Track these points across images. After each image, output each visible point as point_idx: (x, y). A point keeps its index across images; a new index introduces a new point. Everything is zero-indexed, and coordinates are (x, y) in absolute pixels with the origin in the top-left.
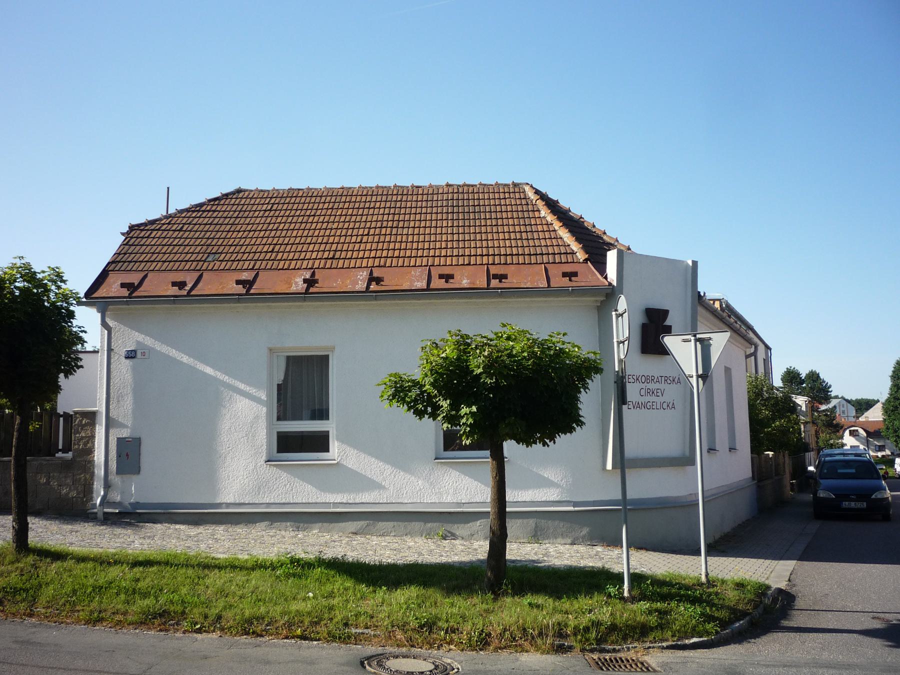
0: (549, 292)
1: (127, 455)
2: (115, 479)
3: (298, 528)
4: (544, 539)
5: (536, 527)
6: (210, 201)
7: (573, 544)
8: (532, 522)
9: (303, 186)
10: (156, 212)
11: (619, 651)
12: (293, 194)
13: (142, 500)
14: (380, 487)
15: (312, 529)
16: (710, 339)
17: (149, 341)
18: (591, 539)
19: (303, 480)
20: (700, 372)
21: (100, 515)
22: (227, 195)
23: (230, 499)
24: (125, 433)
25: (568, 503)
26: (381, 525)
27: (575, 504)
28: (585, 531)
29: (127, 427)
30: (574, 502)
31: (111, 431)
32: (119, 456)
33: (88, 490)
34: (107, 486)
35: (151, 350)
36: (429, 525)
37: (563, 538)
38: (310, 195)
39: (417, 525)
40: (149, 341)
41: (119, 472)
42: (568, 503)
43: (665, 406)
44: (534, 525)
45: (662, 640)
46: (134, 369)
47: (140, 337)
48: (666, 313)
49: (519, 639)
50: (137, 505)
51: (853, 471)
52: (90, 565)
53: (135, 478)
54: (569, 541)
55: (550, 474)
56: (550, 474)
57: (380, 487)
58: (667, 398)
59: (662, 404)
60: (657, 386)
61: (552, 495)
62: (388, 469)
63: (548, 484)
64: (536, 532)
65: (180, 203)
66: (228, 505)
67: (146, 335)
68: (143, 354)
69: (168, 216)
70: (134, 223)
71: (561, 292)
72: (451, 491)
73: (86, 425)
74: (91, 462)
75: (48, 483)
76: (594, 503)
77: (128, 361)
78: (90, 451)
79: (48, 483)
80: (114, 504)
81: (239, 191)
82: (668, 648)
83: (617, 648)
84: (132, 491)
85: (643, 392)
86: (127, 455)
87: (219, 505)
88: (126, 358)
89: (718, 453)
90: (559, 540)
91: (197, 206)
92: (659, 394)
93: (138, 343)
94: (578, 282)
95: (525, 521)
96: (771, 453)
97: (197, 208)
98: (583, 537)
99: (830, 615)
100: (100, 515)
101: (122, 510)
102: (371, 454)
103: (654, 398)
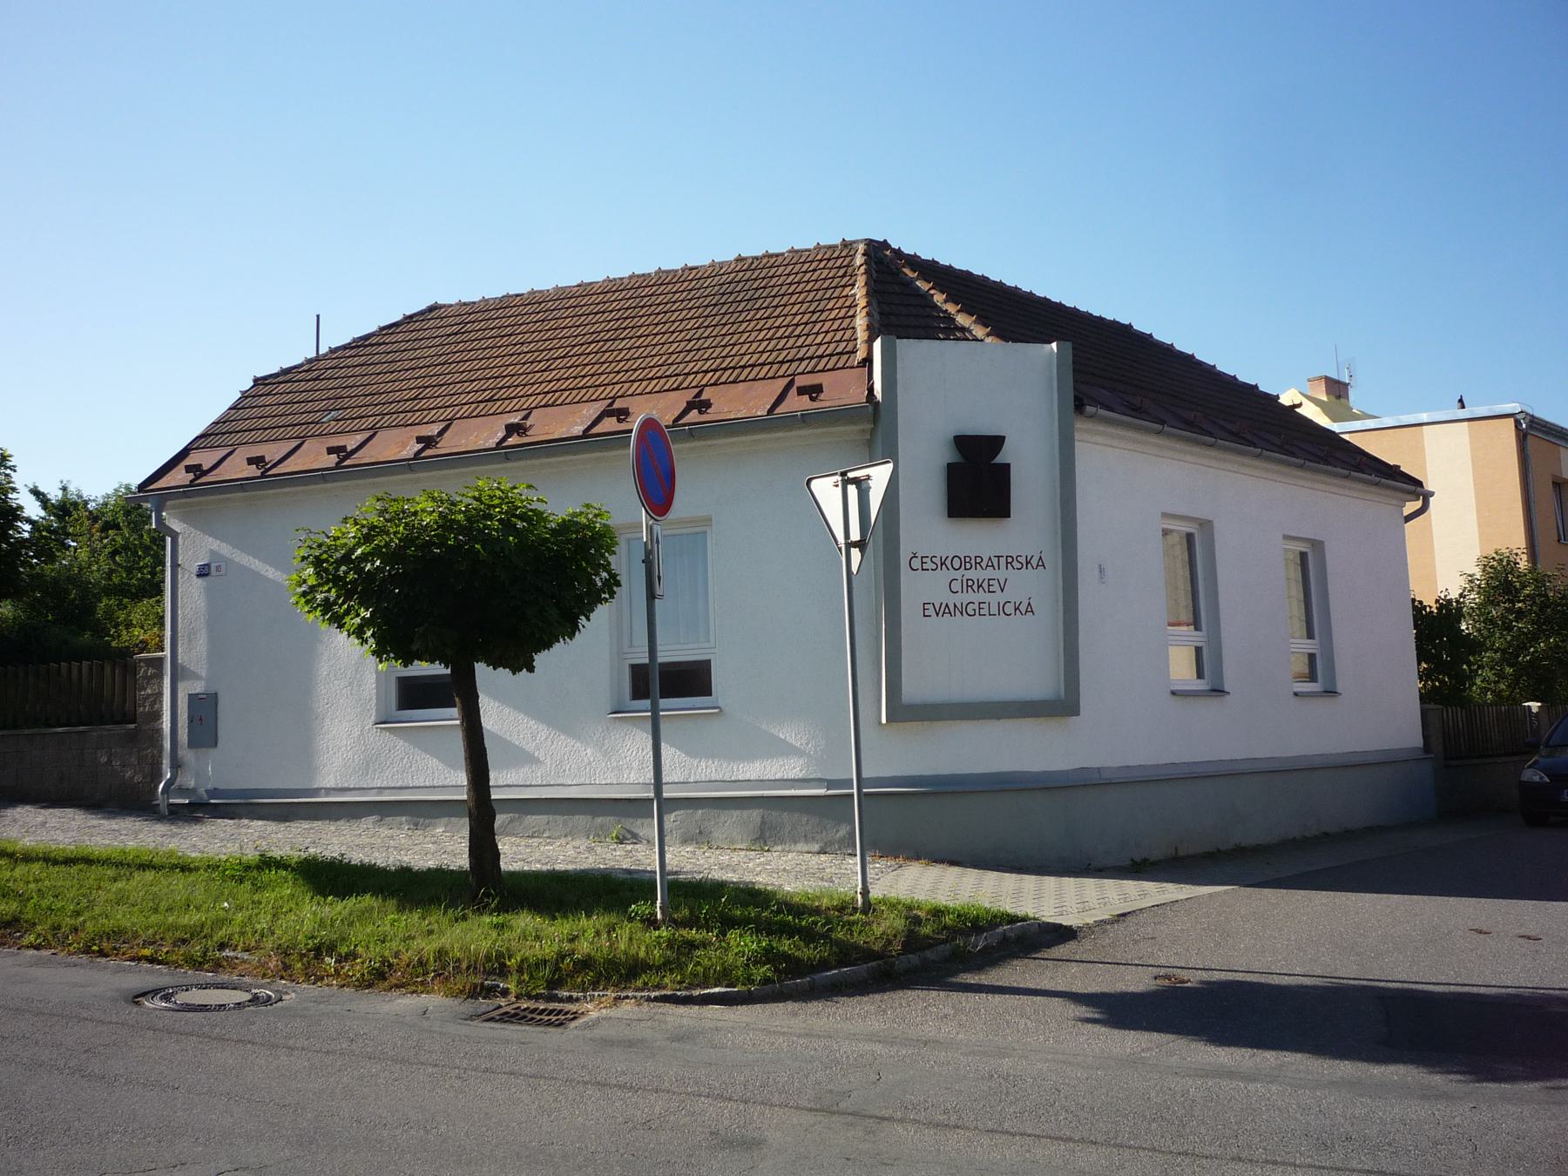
0: (772, 422)
1: (1101, 570)
2: (186, 754)
3: (416, 824)
4: (775, 844)
5: (763, 823)
6: (382, 329)
7: (822, 852)
8: (755, 815)
9: (524, 290)
10: (297, 352)
11: (577, 1000)
12: (507, 303)
13: (222, 786)
14: (532, 760)
15: (435, 826)
16: (869, 477)
17: (225, 549)
19: (426, 751)
20: (855, 535)
21: (164, 809)
22: (411, 317)
23: (329, 782)
24: (198, 687)
25: (819, 782)
26: (531, 820)
29: (197, 677)
30: (828, 781)
31: (181, 686)
32: (191, 720)
33: (156, 775)
34: (176, 765)
35: (228, 561)
36: (599, 820)
37: (807, 841)
38: (535, 301)
39: (581, 820)
40: (225, 549)
41: (192, 744)
42: (819, 782)
43: (1009, 609)
44: (759, 820)
45: (658, 987)
46: (209, 593)
47: (214, 544)
48: (997, 442)
49: (418, 975)
50: (214, 793)
52: (36, 868)
53: (212, 753)
54: (816, 847)
55: (790, 734)
56: (790, 734)
57: (532, 760)
58: (1014, 594)
59: (1002, 609)
60: (990, 573)
61: (792, 768)
62: (543, 731)
63: (787, 750)
64: (762, 831)
65: (336, 337)
66: (329, 791)
67: (222, 540)
68: (218, 568)
69: (317, 359)
70: (259, 375)
71: (805, 419)
72: (635, 765)
73: (151, 677)
74: (159, 731)
75: (109, 762)
77: (200, 581)
78: (157, 716)
79: (109, 762)
80: (183, 791)
81: (432, 309)
82: (656, 999)
83: (575, 995)
84: (209, 771)
85: (956, 586)
86: (1101, 570)
87: (316, 792)
88: (199, 576)
89: (1227, 697)
90: (801, 846)
91: (361, 338)
92: (996, 587)
93: (212, 552)
94: (828, 400)
95: (746, 813)
96: (1535, 706)
97: (362, 343)
99: (1074, 968)
100: (164, 809)
101: (194, 799)
102: (517, 708)
103: (982, 596)
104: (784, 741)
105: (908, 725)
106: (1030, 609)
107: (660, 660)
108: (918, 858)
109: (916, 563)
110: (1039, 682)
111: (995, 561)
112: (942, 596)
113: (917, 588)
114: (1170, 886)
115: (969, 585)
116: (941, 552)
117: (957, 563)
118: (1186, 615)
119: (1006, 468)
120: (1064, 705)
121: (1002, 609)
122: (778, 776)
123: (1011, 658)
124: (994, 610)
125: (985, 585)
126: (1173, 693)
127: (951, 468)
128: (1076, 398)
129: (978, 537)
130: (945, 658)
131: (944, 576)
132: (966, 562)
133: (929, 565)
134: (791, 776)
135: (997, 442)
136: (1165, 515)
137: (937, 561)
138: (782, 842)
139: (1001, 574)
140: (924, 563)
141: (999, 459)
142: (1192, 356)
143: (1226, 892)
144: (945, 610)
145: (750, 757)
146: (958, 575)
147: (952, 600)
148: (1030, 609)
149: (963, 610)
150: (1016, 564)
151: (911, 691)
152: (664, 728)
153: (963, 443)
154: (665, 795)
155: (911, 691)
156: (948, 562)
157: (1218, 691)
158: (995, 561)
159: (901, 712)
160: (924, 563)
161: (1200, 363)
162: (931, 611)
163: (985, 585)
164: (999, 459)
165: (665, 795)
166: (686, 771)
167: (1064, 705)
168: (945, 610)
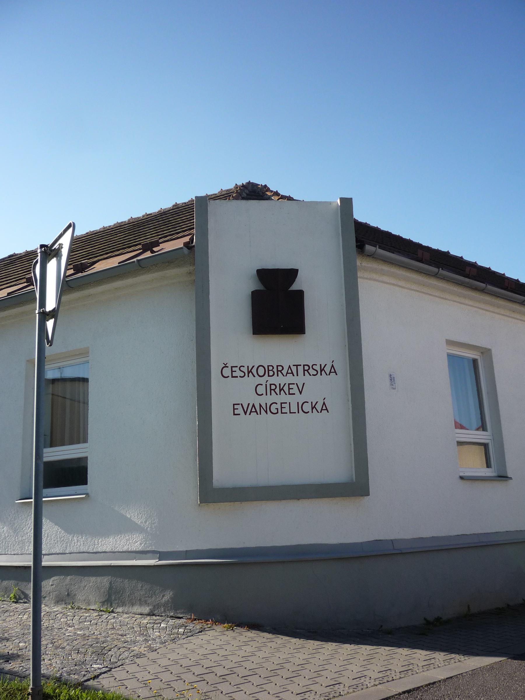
1: (392, 379)
4: (118, 606)
5: (111, 588)
7: (151, 614)
8: (105, 581)
18: (176, 608)
25: (142, 554)
27: (162, 555)
28: (168, 595)
30: (159, 552)
37: (141, 605)
43: (307, 407)
44: (107, 585)
48: (292, 274)
51: (44, 499)
54: (146, 610)
56: (134, 514)
59: (300, 407)
60: (290, 379)
61: (135, 542)
63: (129, 527)
64: (110, 596)
76: (187, 554)
85: (261, 390)
86: (392, 379)
90: (137, 609)
92: (295, 390)
95: (99, 579)
98: (165, 605)
104: (130, 519)
105: (222, 505)
106: (325, 408)
107: (45, 459)
108: (222, 622)
109: (227, 372)
110: (335, 467)
111: (294, 369)
112: (249, 398)
113: (225, 393)
114: (440, 656)
115: (272, 389)
116: (249, 362)
117: (261, 371)
118: (475, 421)
119: (301, 293)
120: (355, 487)
121: (300, 407)
122: (125, 549)
123: (311, 447)
124: (294, 409)
125: (286, 388)
126: (462, 478)
127: (255, 295)
128: (357, 241)
129: (278, 350)
130: (247, 450)
131: (251, 381)
132: (269, 371)
133: (238, 373)
134: (134, 548)
135: (292, 274)
136: (450, 343)
137: (245, 370)
138: (123, 604)
139: (300, 379)
140: (231, 372)
141: (295, 287)
142: (489, 269)
143: (491, 667)
144: (252, 410)
145: (105, 533)
146: (262, 380)
147: (258, 401)
148: (325, 408)
149: (267, 409)
150: (312, 371)
151: (221, 477)
152: (45, 510)
153: (264, 275)
154: (44, 564)
155: (221, 477)
156: (254, 371)
157: (503, 477)
158: (294, 369)
159: (210, 493)
160: (231, 372)
161: (494, 273)
162: (240, 411)
163: (286, 388)
164: (295, 287)
165: (44, 564)
166: (62, 546)
167: (355, 487)
168: (252, 410)
